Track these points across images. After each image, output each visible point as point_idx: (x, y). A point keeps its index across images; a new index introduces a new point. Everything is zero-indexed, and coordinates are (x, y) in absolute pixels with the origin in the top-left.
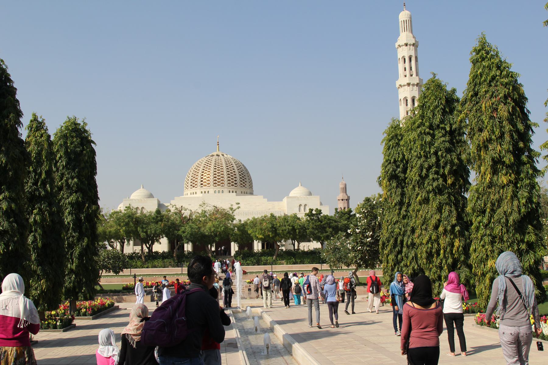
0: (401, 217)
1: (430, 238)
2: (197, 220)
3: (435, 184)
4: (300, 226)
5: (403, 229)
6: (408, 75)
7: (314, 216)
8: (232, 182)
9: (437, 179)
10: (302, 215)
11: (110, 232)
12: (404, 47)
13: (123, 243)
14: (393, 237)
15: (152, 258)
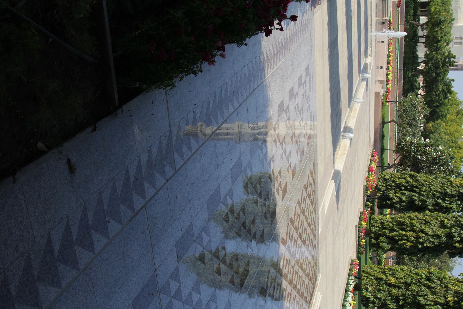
0: (435, 193)
3: (456, 235)
4: (441, 46)
5: (425, 193)
14: (419, 185)
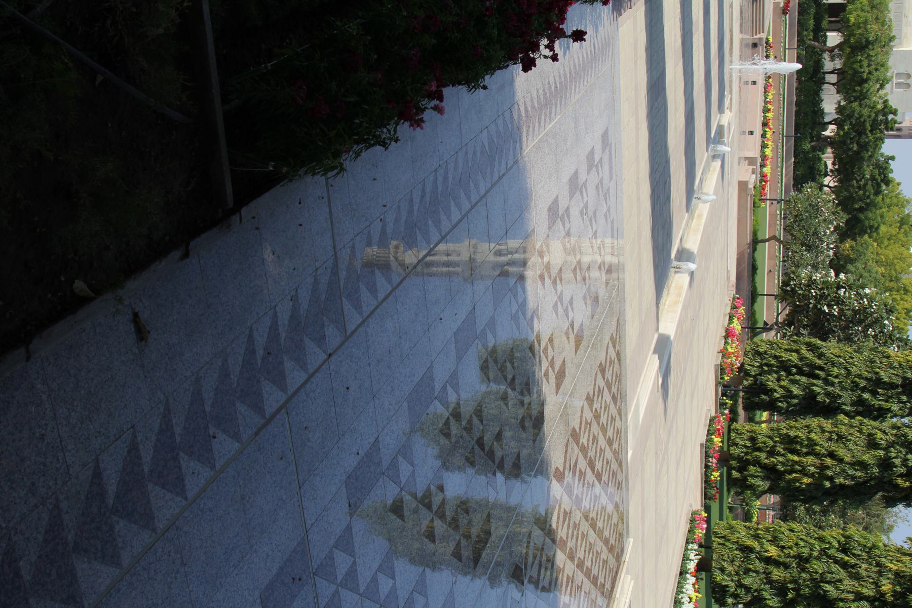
0: (856, 379)
3: (897, 461)
4: (868, 91)
5: (836, 381)
14: (826, 364)
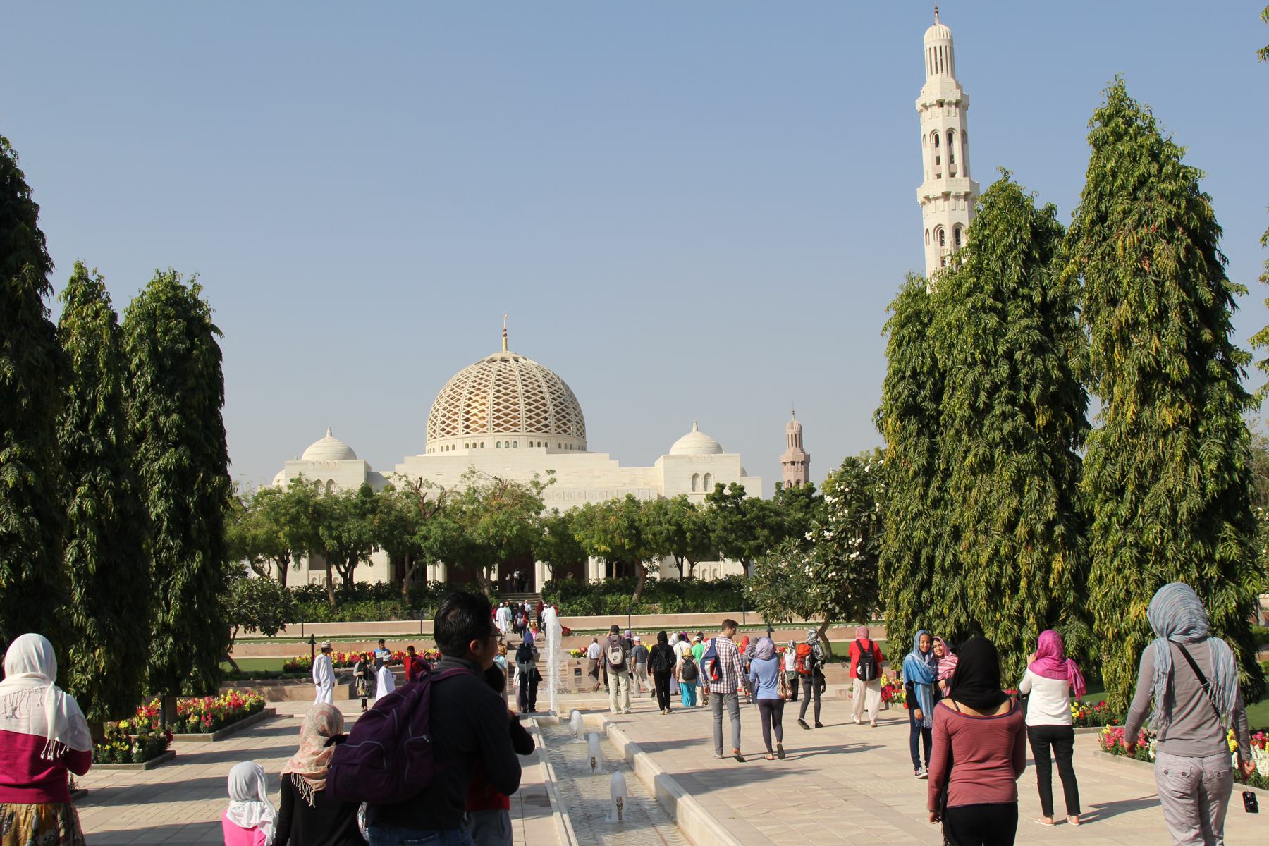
0: (929, 502)
1: (997, 551)
2: (457, 510)
3: (1007, 427)
4: (694, 523)
5: (933, 531)
6: (945, 174)
7: (728, 500)
8: (538, 422)
9: (1013, 415)
10: (699, 498)
11: (255, 538)
12: (935, 108)
13: (286, 563)
14: (909, 549)
15: (352, 598)
